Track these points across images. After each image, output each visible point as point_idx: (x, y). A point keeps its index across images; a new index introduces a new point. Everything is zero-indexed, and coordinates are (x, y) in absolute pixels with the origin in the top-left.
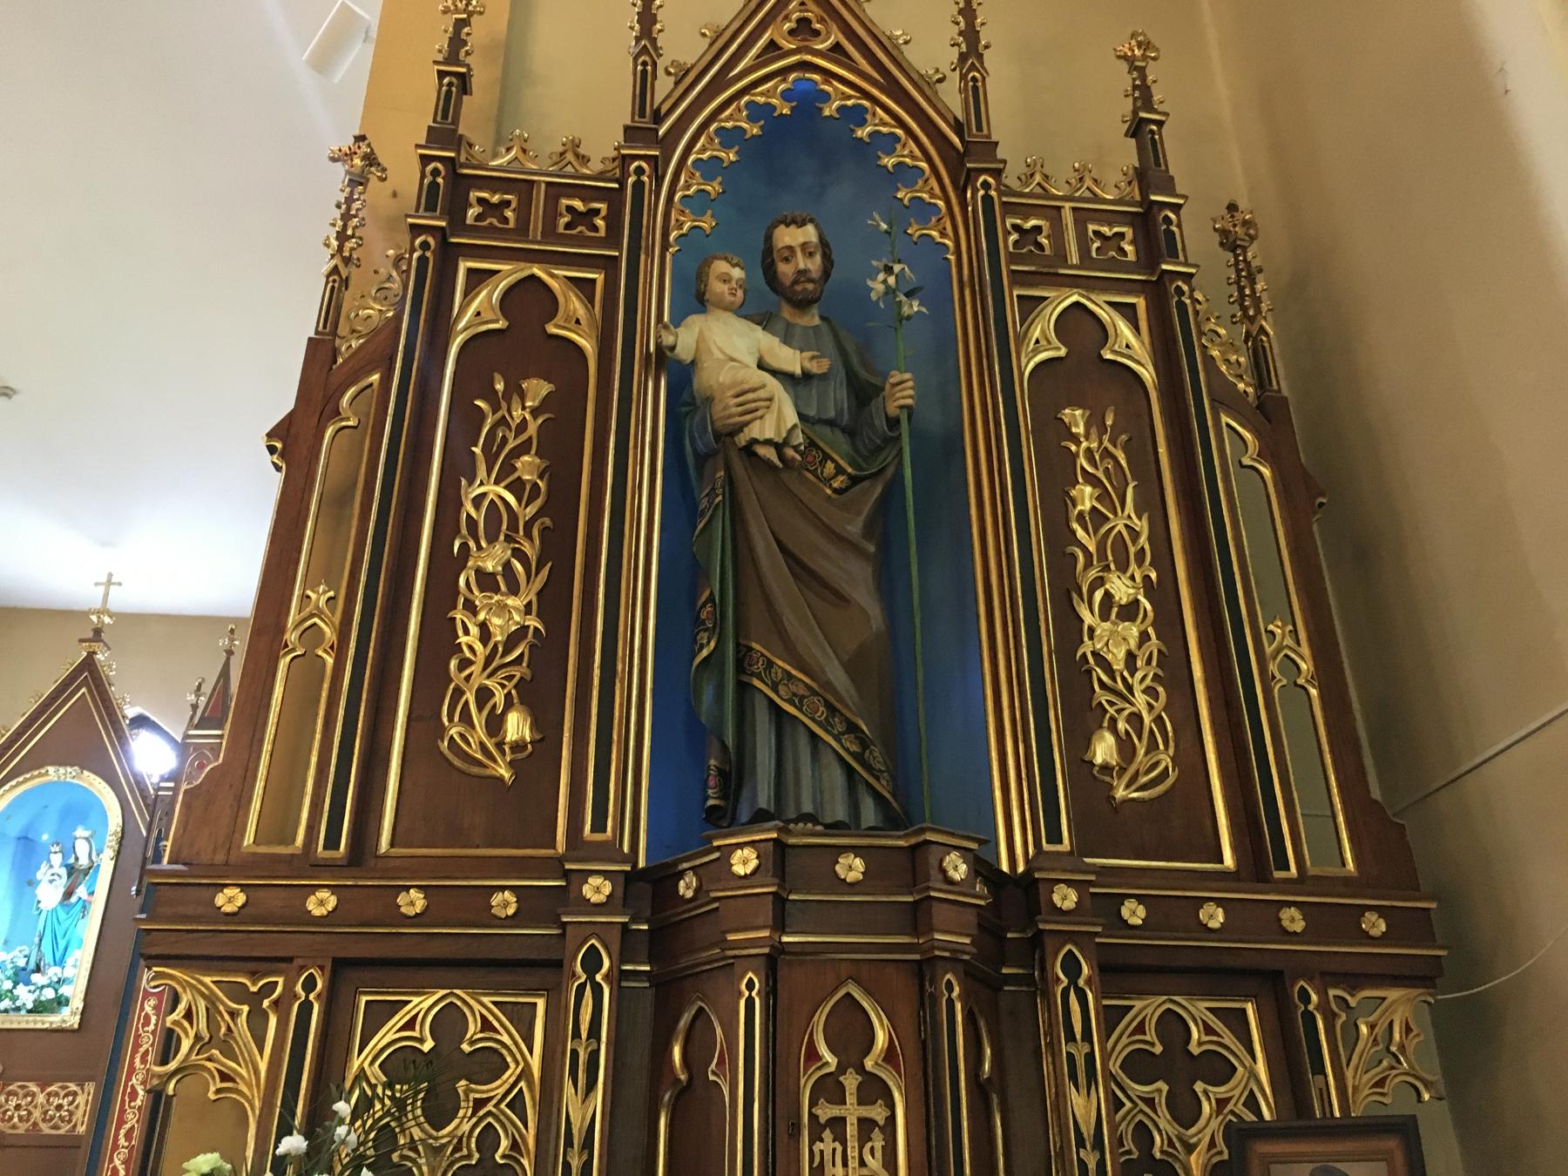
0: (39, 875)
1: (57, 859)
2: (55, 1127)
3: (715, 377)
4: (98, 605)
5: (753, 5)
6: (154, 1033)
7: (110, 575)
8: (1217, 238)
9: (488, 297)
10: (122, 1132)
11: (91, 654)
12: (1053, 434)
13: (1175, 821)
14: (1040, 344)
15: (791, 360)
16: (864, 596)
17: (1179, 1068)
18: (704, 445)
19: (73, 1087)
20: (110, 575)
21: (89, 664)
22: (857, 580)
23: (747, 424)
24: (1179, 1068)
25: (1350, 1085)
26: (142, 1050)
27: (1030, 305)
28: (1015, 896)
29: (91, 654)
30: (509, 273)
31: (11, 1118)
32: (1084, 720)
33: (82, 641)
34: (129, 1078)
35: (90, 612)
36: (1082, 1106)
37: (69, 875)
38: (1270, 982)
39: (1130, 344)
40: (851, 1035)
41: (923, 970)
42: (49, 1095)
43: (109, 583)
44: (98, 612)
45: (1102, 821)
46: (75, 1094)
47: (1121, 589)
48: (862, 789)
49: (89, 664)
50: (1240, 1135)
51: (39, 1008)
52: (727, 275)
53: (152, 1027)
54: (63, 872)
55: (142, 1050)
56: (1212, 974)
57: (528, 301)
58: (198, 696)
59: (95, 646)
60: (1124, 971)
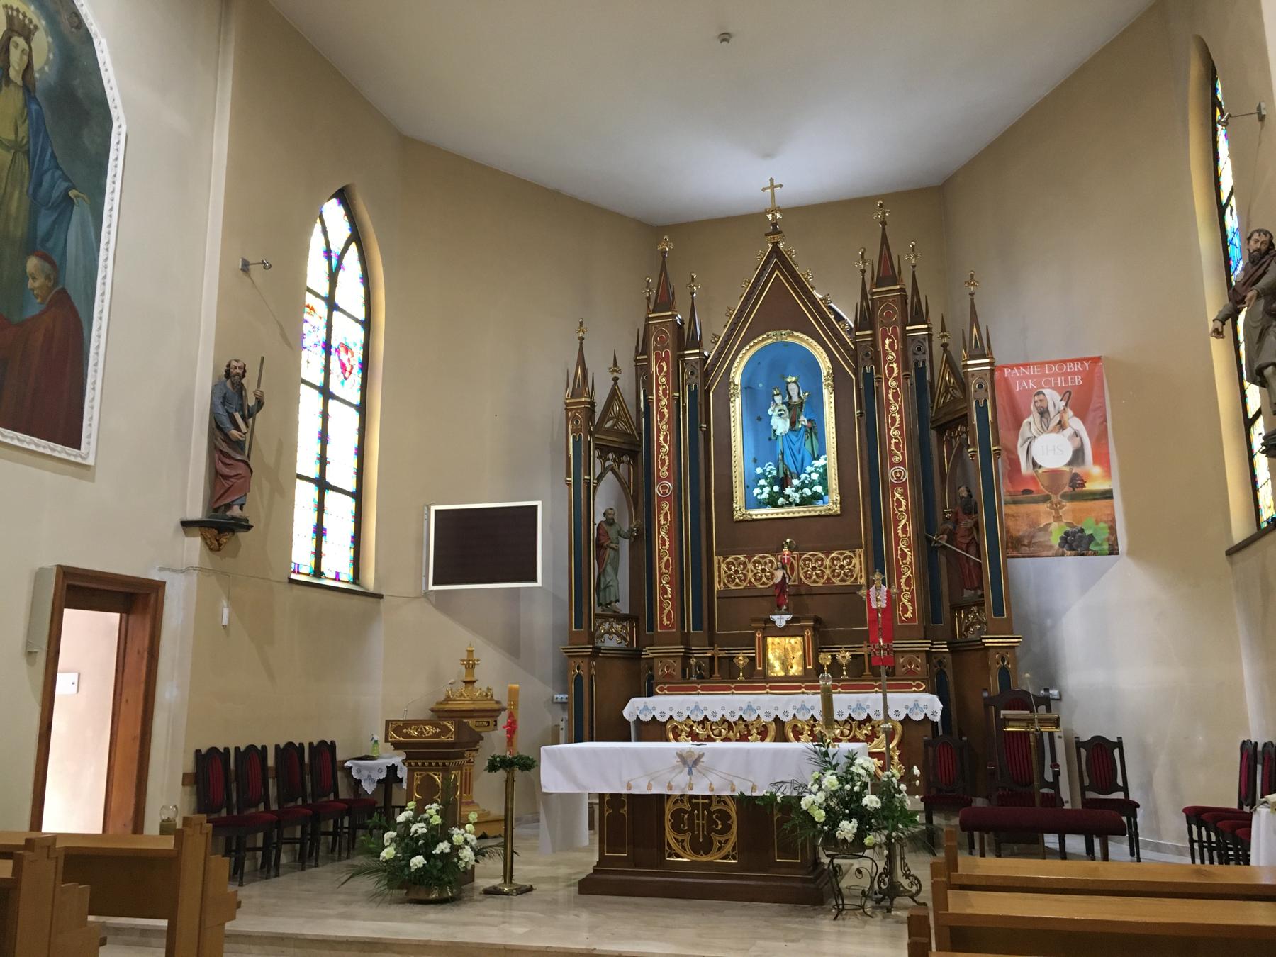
0: (770, 412)
1: (778, 399)
2: (842, 580)
4: (769, 205)
5: (6, 451)
6: (906, 511)
7: (772, 180)
8: (251, 523)
10: (903, 581)
11: (775, 244)
19: (848, 553)
20: (772, 180)
21: (776, 251)
26: (666, 612)
29: (775, 244)
31: (811, 576)
33: (767, 235)
34: (897, 544)
35: (766, 212)
37: (789, 409)
42: (833, 559)
43: (773, 186)
44: (773, 211)
46: (850, 558)
49: (776, 251)
51: (805, 501)
53: (904, 508)
54: (784, 407)
55: (666, 612)
58: (864, 263)
59: (777, 237)
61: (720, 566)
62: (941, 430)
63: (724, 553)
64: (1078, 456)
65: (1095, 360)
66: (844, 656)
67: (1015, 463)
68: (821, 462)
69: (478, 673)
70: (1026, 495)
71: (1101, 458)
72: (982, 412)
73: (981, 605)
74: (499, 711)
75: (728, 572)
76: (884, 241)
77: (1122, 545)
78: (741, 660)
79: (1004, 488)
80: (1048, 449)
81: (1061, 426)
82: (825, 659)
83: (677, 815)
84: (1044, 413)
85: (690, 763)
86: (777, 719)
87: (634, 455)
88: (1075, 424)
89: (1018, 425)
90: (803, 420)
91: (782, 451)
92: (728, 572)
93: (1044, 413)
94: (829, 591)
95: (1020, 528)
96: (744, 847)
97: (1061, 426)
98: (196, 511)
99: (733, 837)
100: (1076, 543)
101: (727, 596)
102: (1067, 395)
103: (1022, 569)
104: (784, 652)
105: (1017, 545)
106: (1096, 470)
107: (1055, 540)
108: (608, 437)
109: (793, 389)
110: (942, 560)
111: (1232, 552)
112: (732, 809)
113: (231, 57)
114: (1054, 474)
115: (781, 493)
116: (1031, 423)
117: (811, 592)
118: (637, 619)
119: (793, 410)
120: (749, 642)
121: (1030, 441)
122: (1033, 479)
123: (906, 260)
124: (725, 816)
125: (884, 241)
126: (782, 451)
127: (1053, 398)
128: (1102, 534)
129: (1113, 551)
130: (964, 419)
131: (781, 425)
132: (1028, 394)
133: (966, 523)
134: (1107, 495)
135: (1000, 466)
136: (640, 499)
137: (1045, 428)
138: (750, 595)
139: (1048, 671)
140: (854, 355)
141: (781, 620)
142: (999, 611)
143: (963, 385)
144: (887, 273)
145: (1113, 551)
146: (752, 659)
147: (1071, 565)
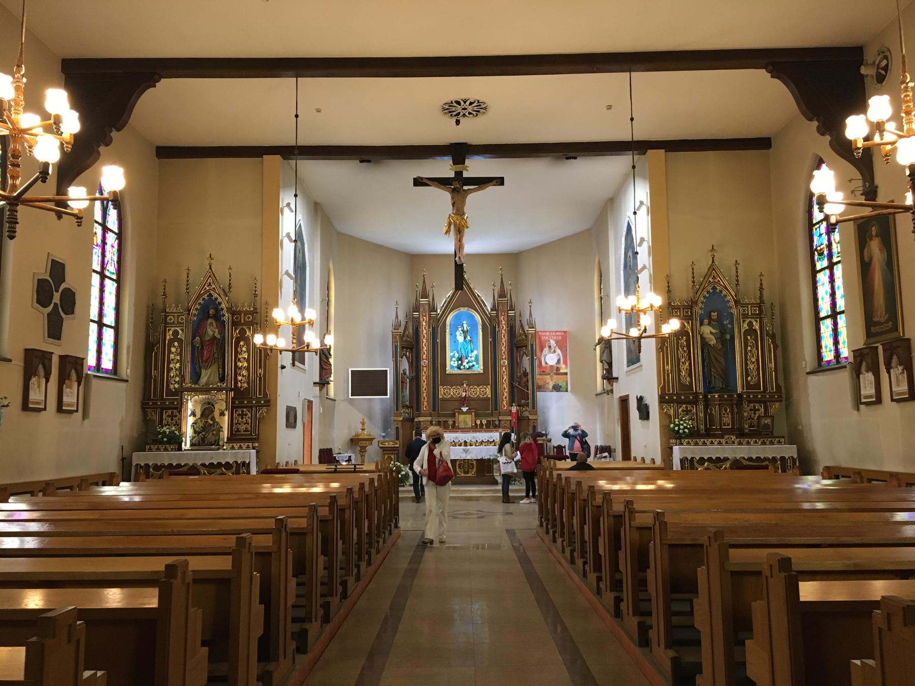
3: (705, 336)
9: (171, 332)
12: (746, 340)
13: (757, 386)
14: (745, 326)
15: (714, 331)
16: (723, 363)
17: (755, 410)
18: (705, 344)
22: (722, 360)
23: (703, 338)
24: (755, 410)
25: (772, 411)
27: (744, 321)
28: (740, 395)
30: (748, 320)
32: (747, 375)
36: (745, 414)
38: (765, 403)
39: (756, 326)
40: (726, 410)
41: (732, 405)
45: (749, 386)
47: (754, 360)
48: (26, 196)
50: (759, 416)
52: (706, 321)
56: (759, 402)
57: (176, 333)
60: (750, 402)
61: (442, 390)
62: (517, 348)
63: (443, 385)
64: (559, 361)
65: (565, 332)
66: (484, 422)
67: (540, 363)
68: (475, 352)
69: (366, 426)
70: (543, 373)
71: (565, 363)
72: (532, 345)
73: (528, 406)
74: (372, 439)
75: (444, 392)
76: (502, 281)
77: (569, 389)
78: (450, 422)
79: (537, 370)
80: (550, 359)
81: (555, 352)
82: (478, 422)
83: (460, 465)
84: (550, 347)
85: (466, 451)
86: (236, 462)
87: (411, 349)
88: (558, 351)
89: (542, 351)
90: (469, 338)
91: (464, 349)
92: (444, 392)
93: (550, 347)
94: (478, 399)
95: (540, 383)
96: (477, 471)
97: (555, 352)
98: (317, 380)
99: (475, 470)
100: (557, 388)
101: (444, 400)
102: (557, 342)
103: (539, 395)
104: (465, 419)
105: (540, 388)
106: (563, 366)
107: (551, 387)
108: (408, 344)
109: (465, 326)
110: (516, 390)
111: (597, 395)
112: (475, 463)
113: (319, 232)
114: (552, 367)
115: (462, 364)
116: (546, 349)
117: (473, 399)
118: (412, 408)
119: (465, 333)
120: (453, 415)
121: (545, 356)
122: (545, 368)
123: (507, 288)
124: (472, 465)
125: (502, 281)
126: (464, 349)
127: (553, 343)
128: (563, 384)
129: (567, 391)
130: (526, 346)
131: (460, 339)
132: (546, 341)
133: (525, 379)
134: (566, 374)
135: (536, 363)
136: (415, 364)
137: (550, 352)
138: (452, 400)
139: (545, 424)
140: (490, 319)
141: (465, 409)
142: (534, 408)
143: (526, 336)
144: (502, 294)
145: (567, 391)
146: (454, 422)
147: (555, 393)
